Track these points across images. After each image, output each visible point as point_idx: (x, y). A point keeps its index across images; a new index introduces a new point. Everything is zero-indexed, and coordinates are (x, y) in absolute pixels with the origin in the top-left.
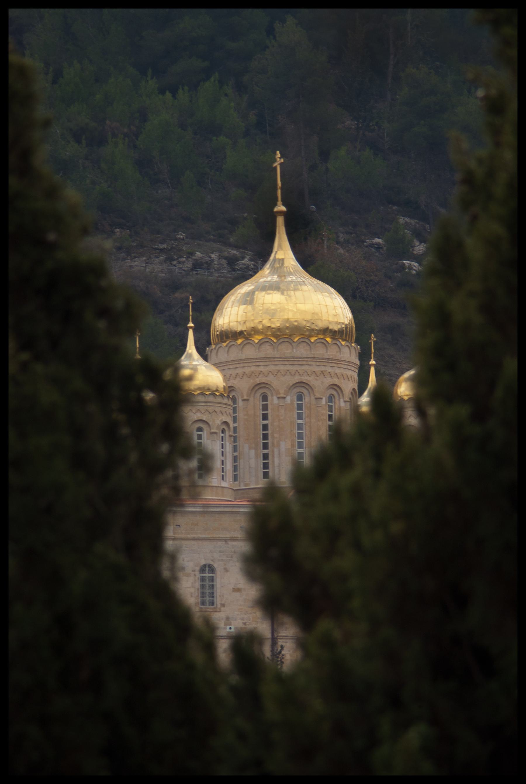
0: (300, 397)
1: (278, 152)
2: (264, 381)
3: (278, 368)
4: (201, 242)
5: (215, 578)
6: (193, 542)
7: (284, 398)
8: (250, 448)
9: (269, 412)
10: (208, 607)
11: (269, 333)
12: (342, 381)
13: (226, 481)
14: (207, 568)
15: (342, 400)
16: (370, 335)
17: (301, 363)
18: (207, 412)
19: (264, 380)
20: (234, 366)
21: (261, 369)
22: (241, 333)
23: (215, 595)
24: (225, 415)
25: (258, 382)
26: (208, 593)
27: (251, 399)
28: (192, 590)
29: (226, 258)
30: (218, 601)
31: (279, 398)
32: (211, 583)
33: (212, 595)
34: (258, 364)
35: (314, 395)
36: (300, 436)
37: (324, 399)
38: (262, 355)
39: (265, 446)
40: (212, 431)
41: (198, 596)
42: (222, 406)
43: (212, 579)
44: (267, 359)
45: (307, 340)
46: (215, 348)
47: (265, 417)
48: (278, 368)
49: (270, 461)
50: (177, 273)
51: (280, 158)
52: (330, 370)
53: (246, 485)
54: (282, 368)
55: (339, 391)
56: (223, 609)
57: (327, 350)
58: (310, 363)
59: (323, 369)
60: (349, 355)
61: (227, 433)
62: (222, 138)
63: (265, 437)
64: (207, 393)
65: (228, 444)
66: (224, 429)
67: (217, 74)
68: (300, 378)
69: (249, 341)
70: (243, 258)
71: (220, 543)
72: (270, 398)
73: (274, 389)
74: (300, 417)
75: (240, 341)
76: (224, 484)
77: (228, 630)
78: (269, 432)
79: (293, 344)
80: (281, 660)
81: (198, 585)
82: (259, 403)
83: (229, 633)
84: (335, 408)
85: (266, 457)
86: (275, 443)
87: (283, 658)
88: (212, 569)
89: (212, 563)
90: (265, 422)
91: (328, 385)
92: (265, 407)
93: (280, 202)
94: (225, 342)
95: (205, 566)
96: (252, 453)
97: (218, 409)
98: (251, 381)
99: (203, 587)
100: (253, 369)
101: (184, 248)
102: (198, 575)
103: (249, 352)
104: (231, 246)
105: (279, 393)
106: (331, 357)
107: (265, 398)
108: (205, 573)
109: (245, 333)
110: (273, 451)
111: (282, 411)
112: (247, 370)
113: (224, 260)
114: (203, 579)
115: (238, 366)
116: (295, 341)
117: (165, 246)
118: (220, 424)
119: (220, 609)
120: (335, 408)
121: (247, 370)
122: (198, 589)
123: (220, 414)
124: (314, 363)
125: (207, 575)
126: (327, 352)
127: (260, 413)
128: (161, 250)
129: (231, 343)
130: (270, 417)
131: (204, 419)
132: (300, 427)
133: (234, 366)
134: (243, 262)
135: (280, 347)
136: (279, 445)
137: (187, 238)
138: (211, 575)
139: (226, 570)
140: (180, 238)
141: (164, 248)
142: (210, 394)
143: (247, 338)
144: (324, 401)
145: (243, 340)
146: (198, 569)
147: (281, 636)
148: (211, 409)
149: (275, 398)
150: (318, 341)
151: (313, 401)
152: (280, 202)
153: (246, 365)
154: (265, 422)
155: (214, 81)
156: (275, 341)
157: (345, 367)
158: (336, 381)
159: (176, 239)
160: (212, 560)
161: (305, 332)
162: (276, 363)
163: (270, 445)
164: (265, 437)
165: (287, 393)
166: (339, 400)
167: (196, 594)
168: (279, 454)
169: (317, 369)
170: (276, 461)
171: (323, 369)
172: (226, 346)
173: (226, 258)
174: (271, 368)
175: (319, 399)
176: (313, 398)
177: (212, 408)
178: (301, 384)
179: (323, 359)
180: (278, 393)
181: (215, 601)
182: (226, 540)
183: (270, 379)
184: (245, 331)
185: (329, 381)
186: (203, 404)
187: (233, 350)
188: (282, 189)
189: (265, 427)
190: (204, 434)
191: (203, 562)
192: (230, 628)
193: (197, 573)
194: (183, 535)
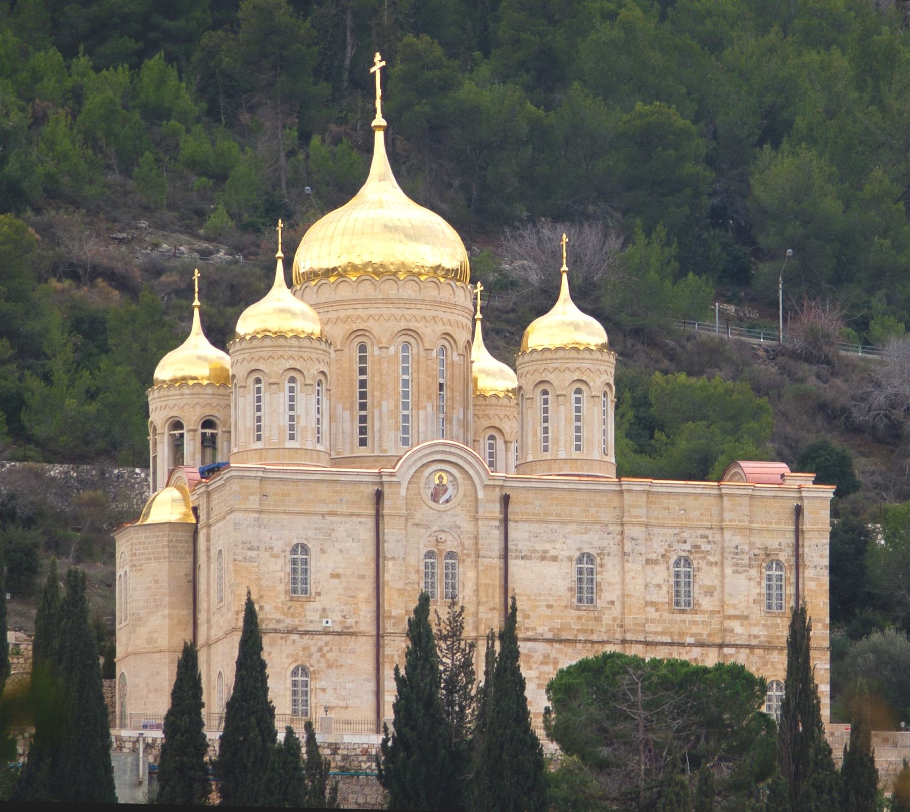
0: (406, 346)
2: (362, 328)
3: (380, 311)
4: (165, 233)
5: (309, 560)
6: (283, 516)
7: (388, 348)
8: (344, 409)
9: (368, 365)
10: (300, 595)
11: (370, 269)
12: (456, 329)
13: (321, 444)
14: (300, 548)
15: (455, 353)
16: (561, 236)
17: (408, 306)
18: (301, 359)
20: (326, 309)
21: (360, 312)
22: (335, 269)
23: (309, 581)
24: (322, 364)
26: (300, 579)
27: (346, 349)
28: (282, 575)
29: (197, 251)
30: (313, 589)
31: (380, 348)
32: (305, 567)
33: (305, 581)
34: (356, 306)
35: (423, 346)
36: (406, 395)
37: (435, 350)
38: (361, 295)
39: (363, 407)
40: (307, 382)
41: (288, 582)
42: (319, 352)
43: (305, 562)
44: (368, 301)
45: (415, 279)
46: (300, 289)
47: (363, 371)
48: (380, 311)
49: (368, 425)
51: (381, 61)
52: (441, 314)
53: (338, 453)
54: (385, 311)
56: (318, 598)
57: (439, 291)
58: (419, 306)
59: (434, 313)
60: (464, 299)
61: (324, 386)
62: (173, 123)
63: (363, 395)
64: (302, 336)
65: (324, 399)
66: (320, 380)
67: (162, 52)
68: (407, 324)
69: (344, 279)
70: (218, 252)
71: (315, 518)
72: (369, 349)
73: (375, 337)
74: (406, 371)
75: (332, 280)
76: (319, 447)
77: (324, 624)
78: (368, 389)
79: (399, 283)
80: (461, 624)
81: (288, 569)
82: (357, 355)
83: (325, 627)
84: (447, 363)
85: (363, 419)
86: (375, 403)
87: (463, 622)
88: (305, 549)
89: (305, 542)
90: (363, 378)
91: (439, 334)
92: (363, 359)
93: (379, 115)
94: (314, 280)
95: (297, 545)
96: (347, 414)
97: (314, 356)
98: (347, 327)
99: (294, 571)
100: (349, 312)
101: (147, 239)
102: (575, 567)
103: (344, 292)
104: (199, 238)
105: (381, 343)
106: (444, 300)
107: (363, 348)
108: (297, 554)
109: (340, 270)
110: (373, 413)
111: (385, 365)
112: (342, 314)
113: (195, 254)
114: (294, 562)
115: (330, 309)
116: (401, 279)
117: (125, 235)
118: (316, 374)
119: (315, 598)
120: (447, 363)
121: (342, 314)
122: (289, 573)
123: (317, 362)
124: (423, 307)
125: (299, 556)
126: (439, 294)
127: (357, 366)
128: (121, 241)
129: (322, 282)
130: (368, 371)
131: (298, 367)
132: (406, 383)
133: (326, 309)
134: (218, 255)
135: (383, 286)
136: (380, 406)
137: (149, 227)
138: (305, 557)
139: (323, 551)
140: (142, 227)
141: (124, 238)
142: (305, 337)
143: (340, 275)
144: (434, 353)
145: (336, 278)
146: (289, 549)
147: (388, 633)
148: (306, 355)
149: (376, 348)
150: (430, 280)
151: (422, 353)
152: (379, 115)
153: (340, 307)
154: (363, 378)
155: (160, 59)
156: (377, 279)
157: (460, 313)
158: (449, 329)
159: (137, 228)
160: (306, 539)
161: (413, 268)
162: (379, 305)
163: (368, 405)
164: (363, 395)
165: (390, 342)
166: (452, 353)
167: (287, 580)
168: (380, 416)
169: (428, 314)
171: (434, 313)
172: (316, 285)
173: (197, 251)
174: (372, 311)
176: (421, 348)
177: (307, 353)
178: (408, 331)
179: (435, 302)
180: (379, 342)
181: (309, 588)
182: (323, 515)
183: (371, 325)
184: (340, 267)
185: (440, 328)
186: (297, 349)
187: (324, 289)
189: (363, 384)
191: (295, 542)
192: (327, 622)
193: (288, 554)
194: (272, 508)
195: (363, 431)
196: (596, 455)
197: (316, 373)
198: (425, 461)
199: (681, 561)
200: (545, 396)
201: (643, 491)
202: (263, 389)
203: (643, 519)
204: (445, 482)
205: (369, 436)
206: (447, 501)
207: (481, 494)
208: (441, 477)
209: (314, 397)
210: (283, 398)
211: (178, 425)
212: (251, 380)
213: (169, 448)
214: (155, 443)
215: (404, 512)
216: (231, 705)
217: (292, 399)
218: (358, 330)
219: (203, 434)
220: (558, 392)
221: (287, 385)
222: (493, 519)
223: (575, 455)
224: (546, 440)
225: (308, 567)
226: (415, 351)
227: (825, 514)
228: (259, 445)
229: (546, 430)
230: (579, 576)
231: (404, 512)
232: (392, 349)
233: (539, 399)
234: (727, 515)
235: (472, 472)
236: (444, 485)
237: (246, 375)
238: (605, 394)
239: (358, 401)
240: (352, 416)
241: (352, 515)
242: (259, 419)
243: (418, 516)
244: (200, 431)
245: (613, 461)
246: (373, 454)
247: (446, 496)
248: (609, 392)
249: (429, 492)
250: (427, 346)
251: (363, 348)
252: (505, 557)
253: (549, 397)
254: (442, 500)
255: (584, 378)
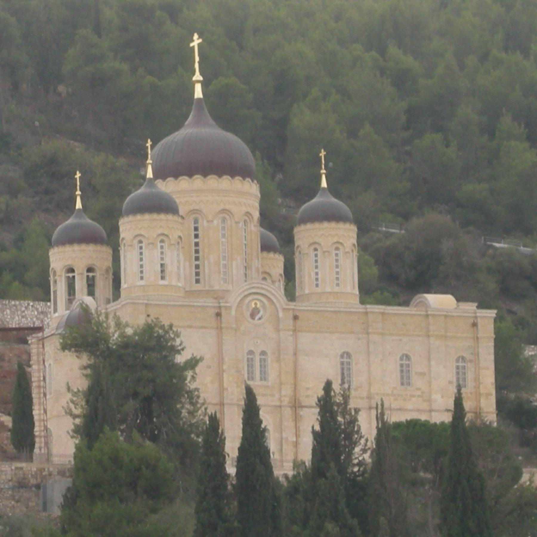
0: (224, 220)
1: (149, 140)
5: (410, 364)
7: (212, 221)
19: (197, 207)
25: (192, 209)
31: (208, 221)
39: (197, 259)
43: (408, 366)
47: (196, 236)
49: (201, 270)
50: (52, 395)
51: (198, 39)
55: (250, 217)
63: (197, 252)
72: (200, 221)
76: (180, 284)
85: (197, 267)
88: (408, 357)
93: (197, 73)
107: (196, 221)
127: (193, 233)
130: (200, 236)
149: (205, 221)
152: (197, 73)
164: (197, 252)
170: (207, 271)
175: (237, 223)
178: (224, 211)
185: (244, 209)
188: (199, 62)
189: (197, 244)
190: (165, 245)
195: (197, 274)
196: (349, 289)
197: (177, 237)
198: (246, 293)
199: (459, 359)
200: (316, 252)
201: (380, 313)
202: (144, 248)
203: (380, 331)
204: (258, 306)
205: (201, 277)
206: (260, 319)
207: (281, 314)
208: (256, 304)
209: (175, 253)
210: (157, 253)
211: (72, 270)
212: (136, 242)
213: (65, 286)
214: (55, 282)
215: (234, 326)
216: (241, 450)
217: (162, 253)
218: (194, 210)
219: (88, 276)
220: (325, 250)
221: (159, 245)
222: (288, 330)
223: (337, 289)
224: (317, 279)
225: (410, 368)
226: (229, 222)
227: (491, 327)
228: (142, 283)
229: (317, 274)
230: (457, 371)
231: (234, 326)
232: (215, 222)
233: (312, 254)
234: (431, 328)
235: (275, 301)
236: (258, 309)
237: (132, 238)
238: (352, 251)
239: (194, 255)
240: (191, 266)
241: (203, 327)
242: (142, 266)
243: (242, 328)
244: (86, 274)
245: (358, 293)
246: (204, 289)
247: (259, 316)
248: (354, 250)
249: (249, 314)
250: (236, 220)
251: (196, 221)
252: (295, 354)
253: (143, 245)
254: (257, 317)
255: (341, 241)
